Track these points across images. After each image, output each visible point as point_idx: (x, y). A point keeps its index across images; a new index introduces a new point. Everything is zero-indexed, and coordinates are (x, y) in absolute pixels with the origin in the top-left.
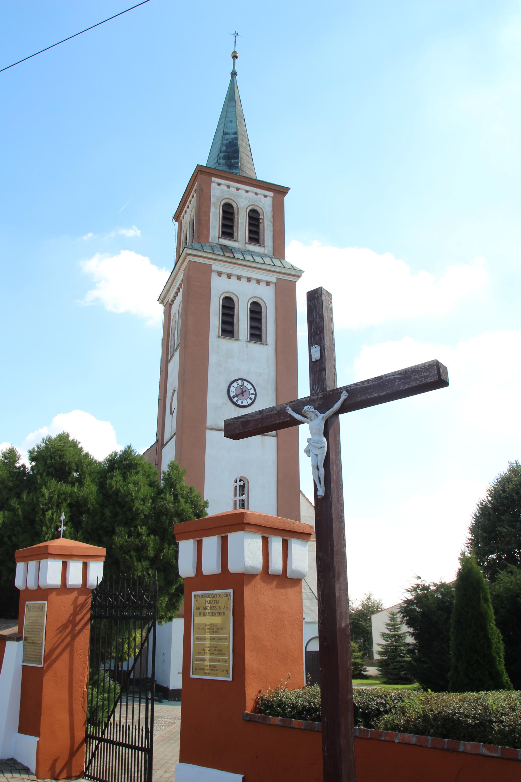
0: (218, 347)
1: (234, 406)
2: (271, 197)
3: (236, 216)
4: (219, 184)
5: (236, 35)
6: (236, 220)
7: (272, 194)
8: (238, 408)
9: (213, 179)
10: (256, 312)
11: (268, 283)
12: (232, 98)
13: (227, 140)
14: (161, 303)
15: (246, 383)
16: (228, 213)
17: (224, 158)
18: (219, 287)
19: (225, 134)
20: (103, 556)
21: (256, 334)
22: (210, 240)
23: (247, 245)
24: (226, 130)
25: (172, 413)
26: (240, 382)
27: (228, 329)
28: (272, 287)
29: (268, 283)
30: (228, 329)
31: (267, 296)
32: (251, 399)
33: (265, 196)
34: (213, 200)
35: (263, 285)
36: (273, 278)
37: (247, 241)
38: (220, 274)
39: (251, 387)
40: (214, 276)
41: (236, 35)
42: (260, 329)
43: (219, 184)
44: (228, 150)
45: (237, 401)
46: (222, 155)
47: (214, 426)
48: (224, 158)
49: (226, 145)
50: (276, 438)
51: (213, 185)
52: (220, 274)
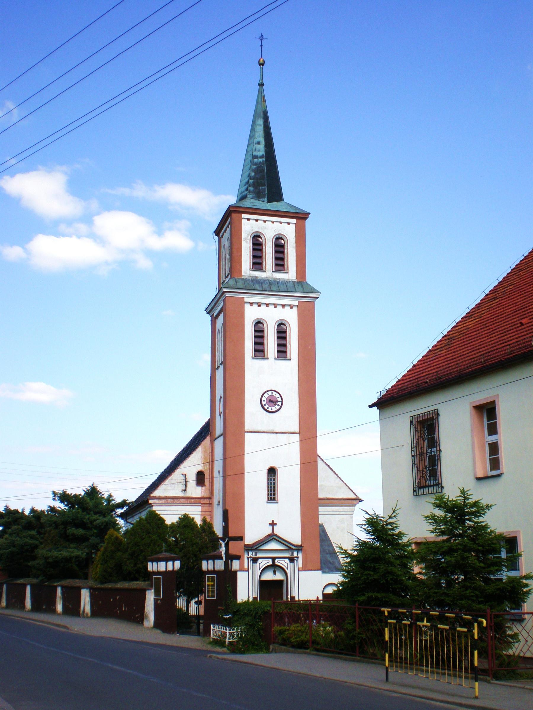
0: (252, 366)
1: (265, 412)
2: (219, 434)
3: (264, 247)
4: (249, 220)
5: (261, 38)
6: (264, 250)
7: (294, 221)
8: (268, 414)
9: (244, 216)
10: (282, 333)
11: (291, 307)
12: (262, 99)
13: (256, 164)
14: (208, 313)
15: (274, 393)
16: (257, 243)
17: (254, 185)
18: (251, 314)
19: (255, 157)
20: (248, 432)
21: (282, 352)
22: (243, 274)
23: (274, 274)
24: (254, 153)
25: (220, 415)
26: (270, 393)
27: (260, 351)
28: (295, 309)
29: (291, 307)
30: (260, 351)
31: (291, 317)
32: (278, 405)
33: (289, 224)
34: (244, 235)
35: (287, 308)
36: (295, 302)
37: (274, 270)
38: (251, 304)
39: (279, 396)
40: (247, 306)
41: (261, 38)
42: (285, 346)
43: (249, 220)
44: (257, 176)
45: (268, 408)
46: (251, 181)
47: (251, 430)
48: (254, 185)
49: (254, 171)
50: (298, 435)
51: (244, 221)
52: (251, 304)
